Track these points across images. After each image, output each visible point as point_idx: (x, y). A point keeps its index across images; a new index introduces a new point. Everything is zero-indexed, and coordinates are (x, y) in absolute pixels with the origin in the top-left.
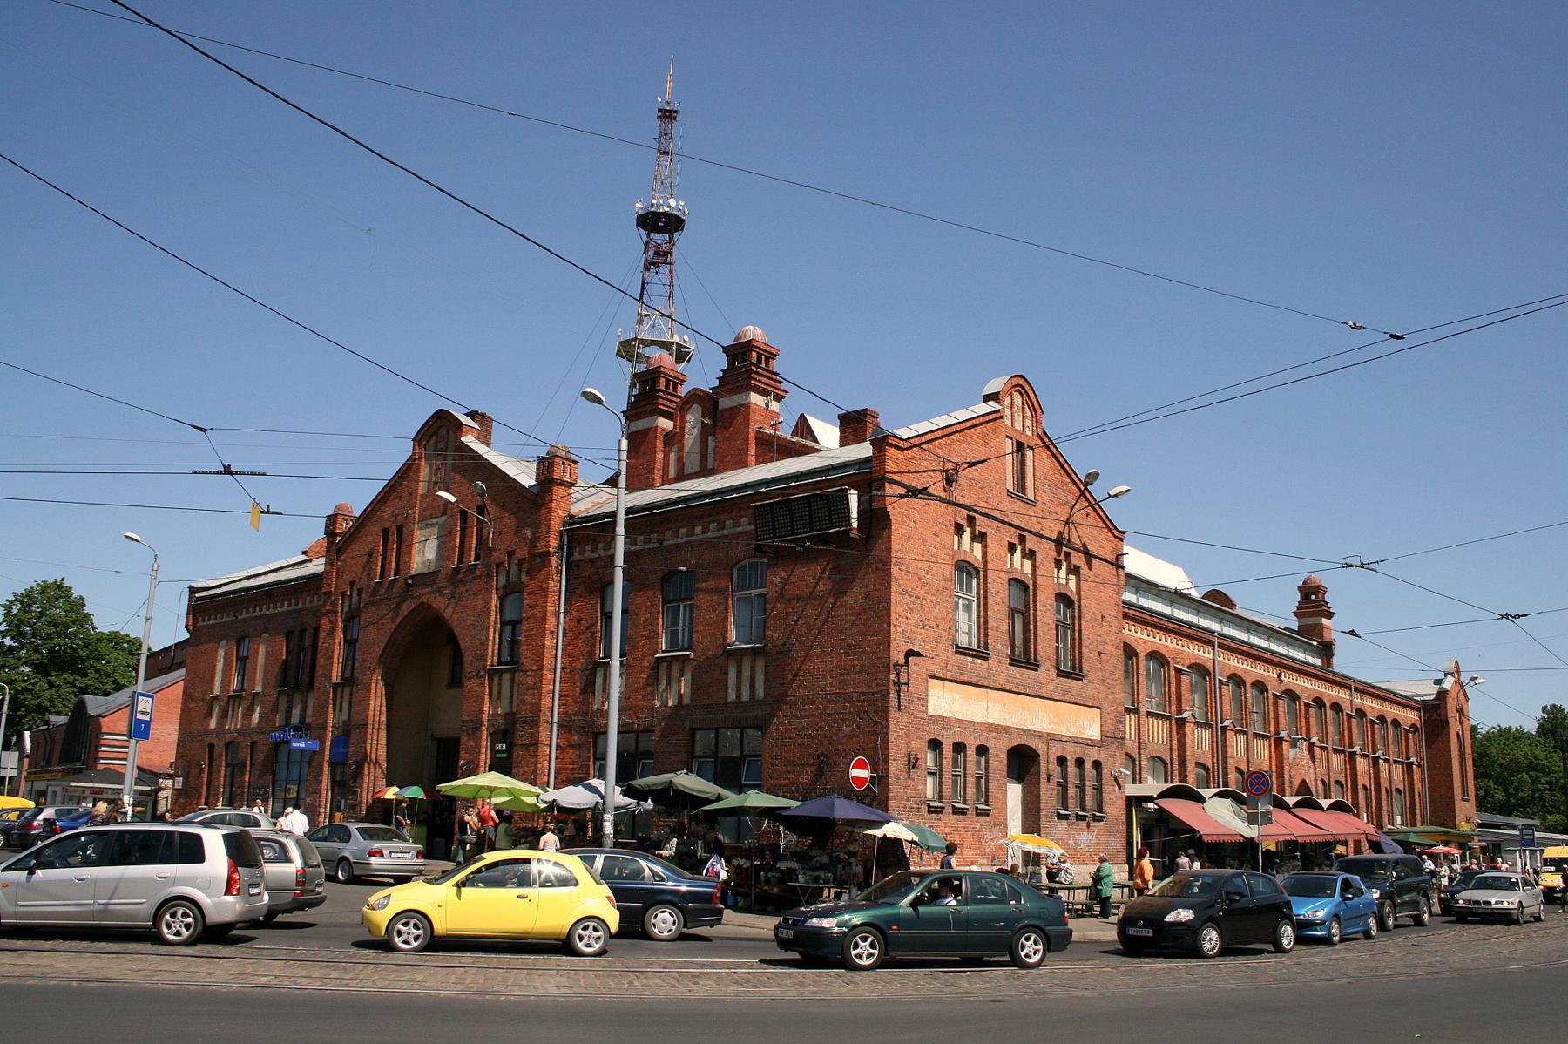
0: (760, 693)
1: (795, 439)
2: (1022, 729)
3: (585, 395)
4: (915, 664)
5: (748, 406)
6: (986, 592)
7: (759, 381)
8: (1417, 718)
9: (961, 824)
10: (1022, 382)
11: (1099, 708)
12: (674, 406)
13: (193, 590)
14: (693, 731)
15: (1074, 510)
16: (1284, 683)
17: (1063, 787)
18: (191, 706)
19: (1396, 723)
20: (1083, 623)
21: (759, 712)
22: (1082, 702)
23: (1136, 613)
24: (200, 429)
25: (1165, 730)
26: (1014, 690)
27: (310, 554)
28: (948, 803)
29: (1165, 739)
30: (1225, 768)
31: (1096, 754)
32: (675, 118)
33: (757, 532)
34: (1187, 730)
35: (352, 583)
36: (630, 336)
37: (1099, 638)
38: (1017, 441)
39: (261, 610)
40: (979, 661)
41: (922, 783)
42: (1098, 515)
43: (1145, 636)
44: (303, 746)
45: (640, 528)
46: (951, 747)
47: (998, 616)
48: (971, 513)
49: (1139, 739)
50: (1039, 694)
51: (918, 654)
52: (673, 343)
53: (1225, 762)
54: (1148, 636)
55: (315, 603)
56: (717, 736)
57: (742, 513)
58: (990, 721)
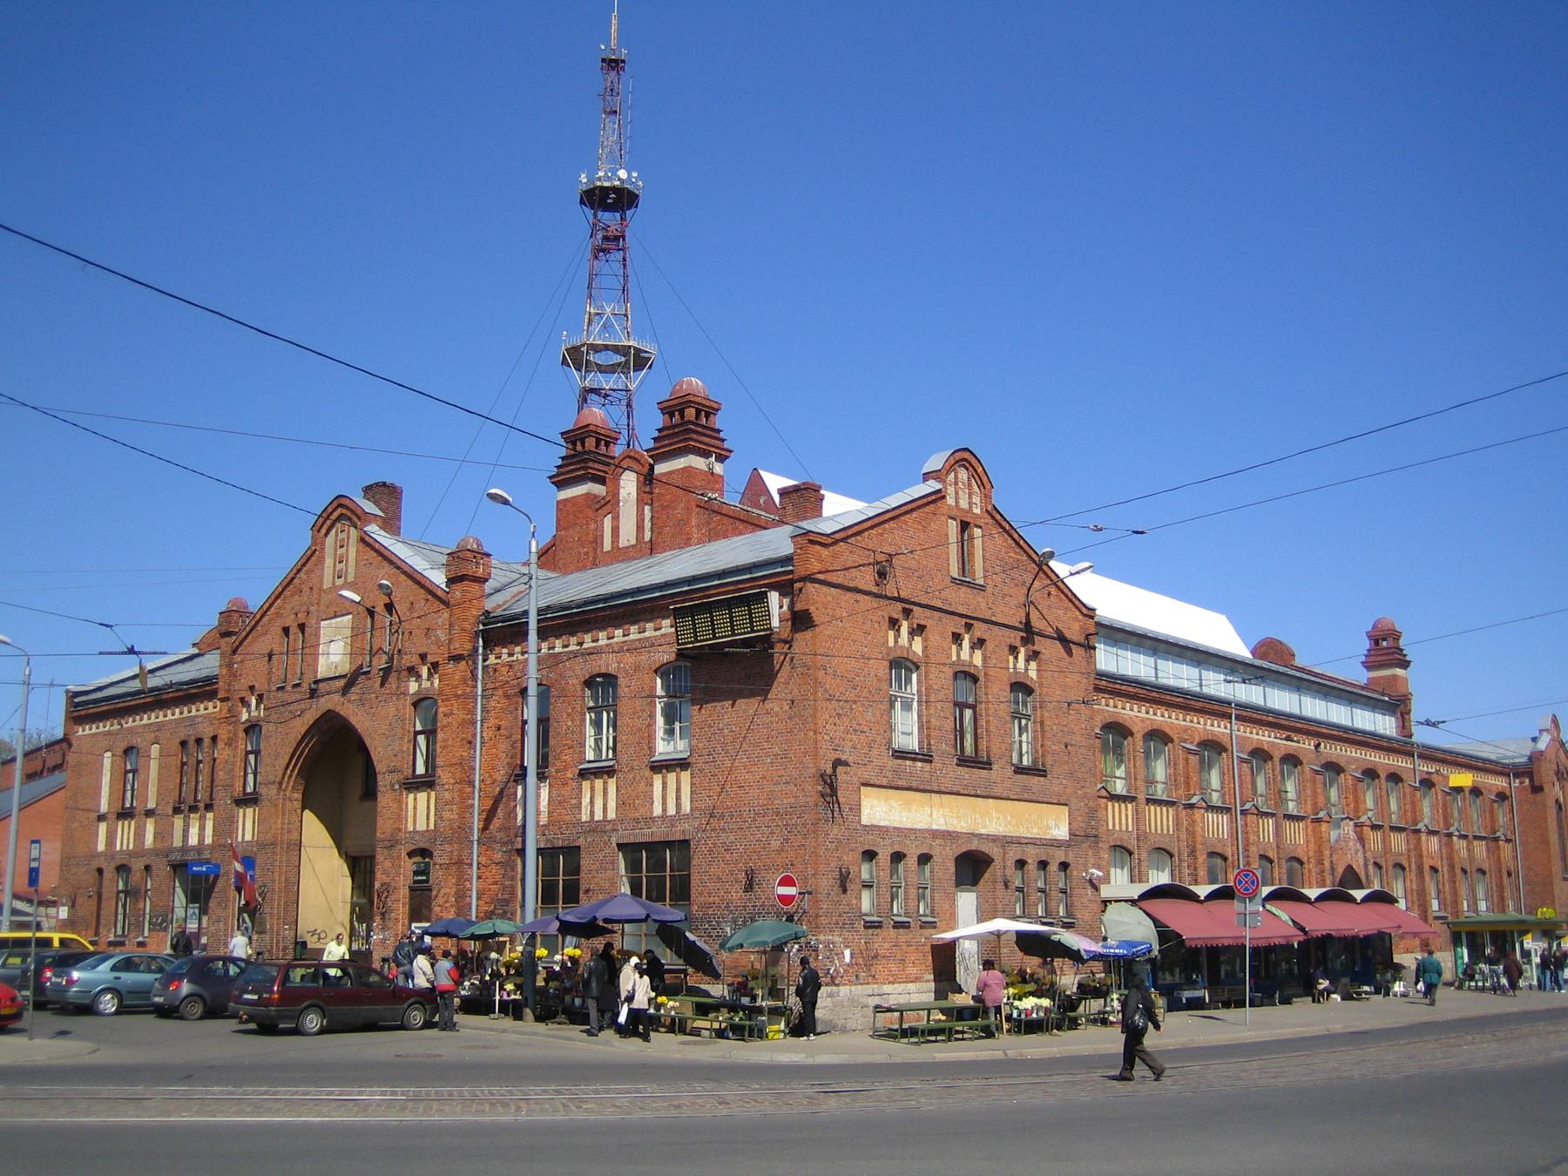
2: (972, 834)
3: (490, 496)
8: (1505, 785)
9: (903, 939)
10: (966, 455)
11: (1067, 805)
18: (74, 826)
22: (1045, 800)
23: (1131, 689)
24: (107, 626)
25: (1171, 818)
26: (962, 792)
32: (623, 69)
33: (678, 636)
35: (252, 688)
37: (1065, 729)
38: (961, 521)
41: (856, 898)
42: (1063, 592)
43: (1143, 715)
44: (204, 869)
48: (907, 606)
51: (846, 764)
52: (630, 347)
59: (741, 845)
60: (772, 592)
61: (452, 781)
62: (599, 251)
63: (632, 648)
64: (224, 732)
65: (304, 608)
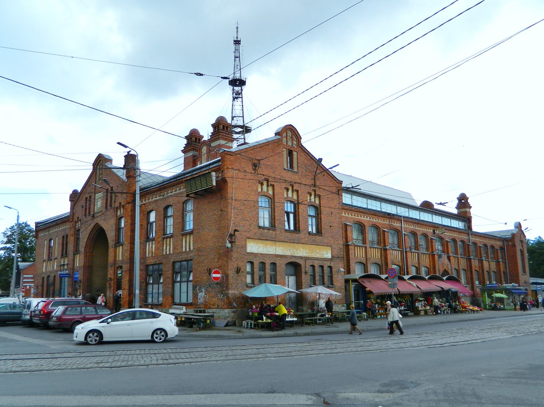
16: (436, 234)
19: (492, 247)
21: (191, 255)
29: (379, 257)
32: (240, 44)
37: (330, 221)
38: (289, 150)
47: (280, 215)
49: (367, 257)
51: (237, 231)
54: (370, 219)
56: (181, 264)
58: (277, 253)
60: (213, 172)
61: (127, 243)
62: (234, 99)
63: (176, 195)
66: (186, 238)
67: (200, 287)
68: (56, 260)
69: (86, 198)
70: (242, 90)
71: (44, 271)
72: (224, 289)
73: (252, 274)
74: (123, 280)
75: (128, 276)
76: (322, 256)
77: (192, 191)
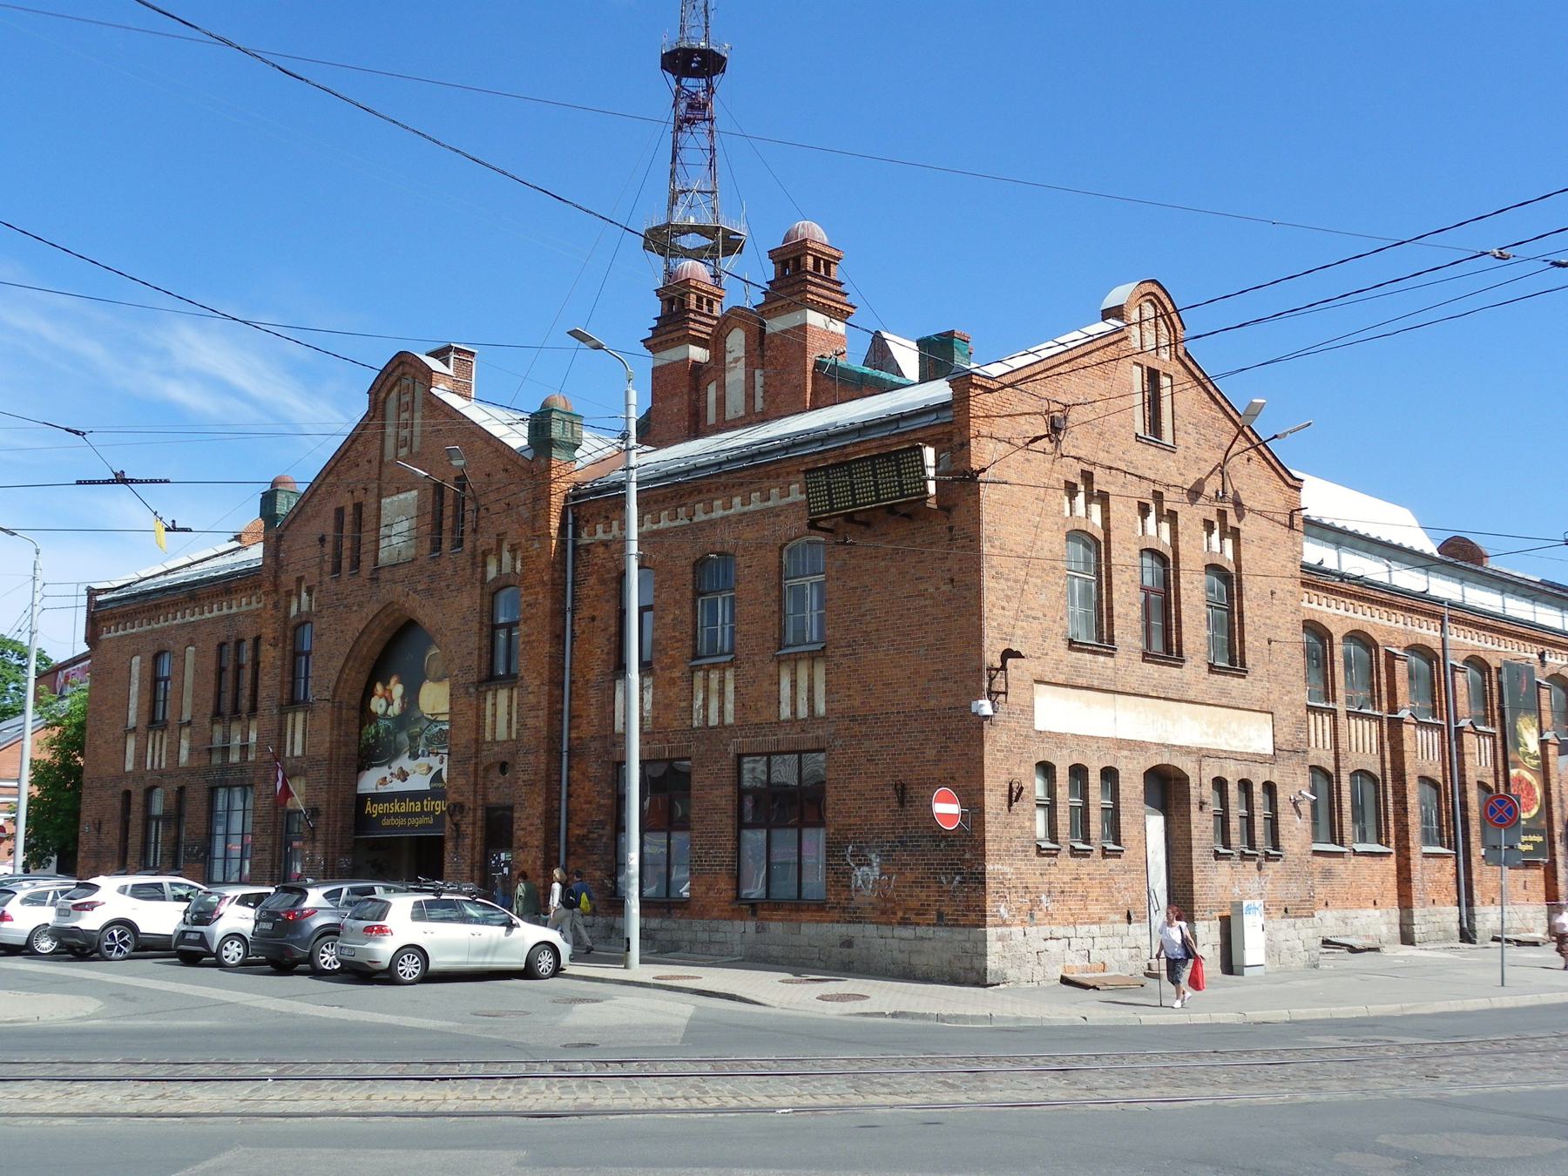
0: (821, 708)
1: (867, 370)
4: (1016, 667)
5: (803, 327)
6: (1109, 569)
7: (816, 294)
10: (1155, 289)
12: (709, 330)
13: (92, 593)
14: (740, 757)
15: (1230, 454)
17: (1223, 820)
20: (1245, 603)
21: (820, 732)
24: (77, 433)
27: (245, 538)
28: (1065, 843)
30: (1463, 783)
31: (1268, 773)
34: (1404, 735)
36: (659, 220)
39: (183, 617)
40: (1101, 658)
43: (1342, 612)
45: (663, 501)
46: (1068, 772)
47: (1127, 600)
50: (1186, 697)
51: (1018, 655)
52: (718, 228)
53: (1462, 775)
54: (1347, 610)
55: (254, 605)
57: (791, 478)
59: (888, 755)
60: (927, 448)
64: (269, 631)
65: (360, 486)
66: (794, 673)
67: (861, 849)
68: (187, 731)
69: (340, 512)
70: (710, 89)
71: (129, 767)
72: (967, 856)
73: (1051, 808)
74: (516, 815)
75: (540, 799)
76: (1245, 747)
77: (832, 510)
